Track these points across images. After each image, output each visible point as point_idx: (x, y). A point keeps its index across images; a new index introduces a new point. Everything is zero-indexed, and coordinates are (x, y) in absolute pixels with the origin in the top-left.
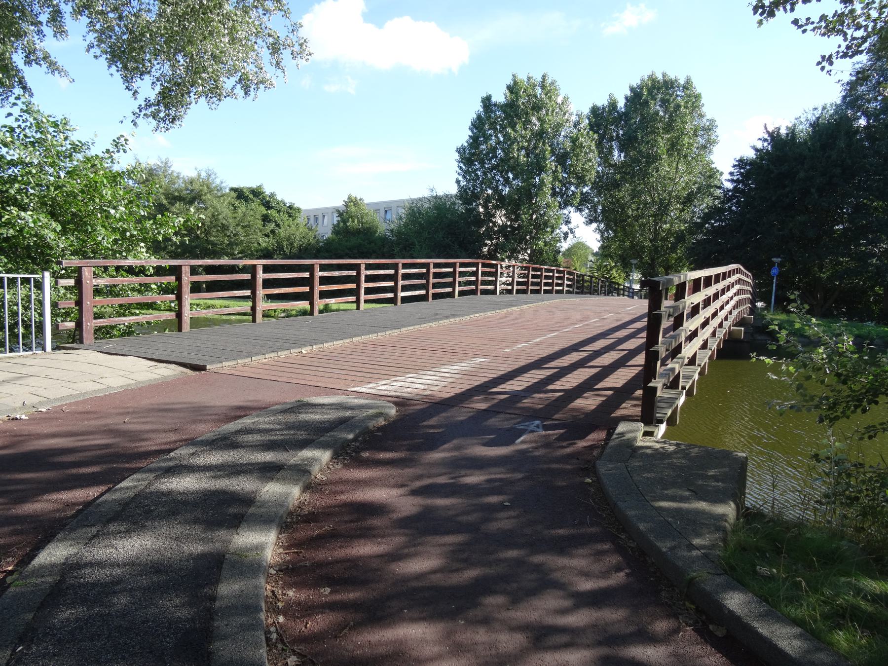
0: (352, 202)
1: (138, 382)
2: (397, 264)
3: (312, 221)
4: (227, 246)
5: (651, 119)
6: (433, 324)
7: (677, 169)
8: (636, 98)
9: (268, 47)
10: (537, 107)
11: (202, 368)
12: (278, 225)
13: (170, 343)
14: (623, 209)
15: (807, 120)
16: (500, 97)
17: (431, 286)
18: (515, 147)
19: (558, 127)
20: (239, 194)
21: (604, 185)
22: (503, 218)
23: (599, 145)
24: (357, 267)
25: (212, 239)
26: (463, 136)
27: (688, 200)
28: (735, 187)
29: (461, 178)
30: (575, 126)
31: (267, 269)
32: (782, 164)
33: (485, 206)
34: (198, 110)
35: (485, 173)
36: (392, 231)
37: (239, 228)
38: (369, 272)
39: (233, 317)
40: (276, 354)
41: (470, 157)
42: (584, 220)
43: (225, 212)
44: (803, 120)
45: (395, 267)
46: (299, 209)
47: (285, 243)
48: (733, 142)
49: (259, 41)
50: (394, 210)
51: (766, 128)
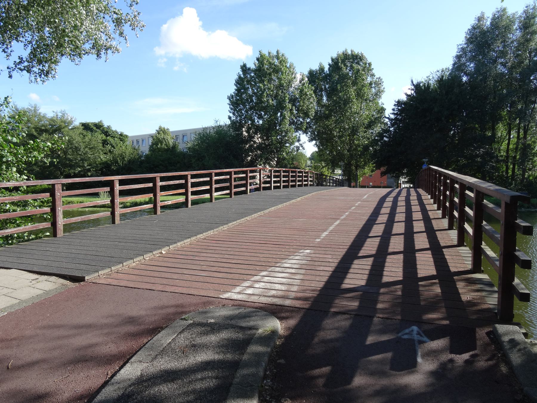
0: (162, 131)
1: (21, 301)
2: (211, 174)
3: (135, 143)
4: (79, 161)
5: (344, 77)
6: (248, 218)
7: (361, 107)
8: (335, 65)
9: (113, 21)
10: (277, 70)
11: (80, 279)
12: (113, 147)
13: (49, 251)
14: (331, 132)
15: (433, 78)
16: (252, 65)
17: (233, 187)
18: (265, 94)
19: (290, 82)
20: (86, 127)
21: (318, 118)
22: (259, 139)
23: (315, 92)
24: (185, 177)
25: (69, 156)
26: (232, 89)
27: (370, 125)
28: (396, 118)
29: (231, 115)
30: (300, 82)
31: (122, 182)
32: (424, 103)
33: (248, 132)
34: (64, 65)
35: (247, 111)
36: (189, 148)
37: (86, 149)
38: (194, 180)
39: (87, 209)
40: (142, 258)
41: (236, 102)
42: (307, 139)
43: (77, 139)
44: (430, 78)
45: (210, 175)
46: (127, 136)
47: (118, 159)
48: (393, 91)
49: (107, 17)
50: (189, 135)
51: (412, 82)
